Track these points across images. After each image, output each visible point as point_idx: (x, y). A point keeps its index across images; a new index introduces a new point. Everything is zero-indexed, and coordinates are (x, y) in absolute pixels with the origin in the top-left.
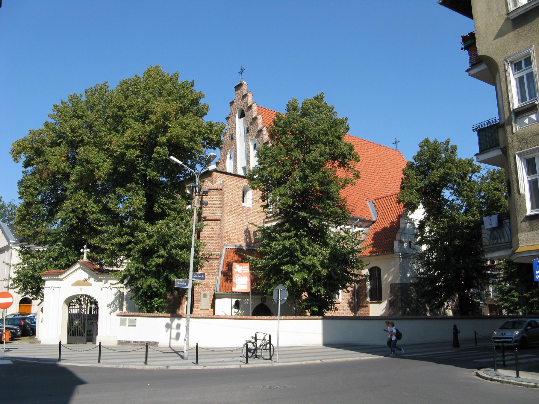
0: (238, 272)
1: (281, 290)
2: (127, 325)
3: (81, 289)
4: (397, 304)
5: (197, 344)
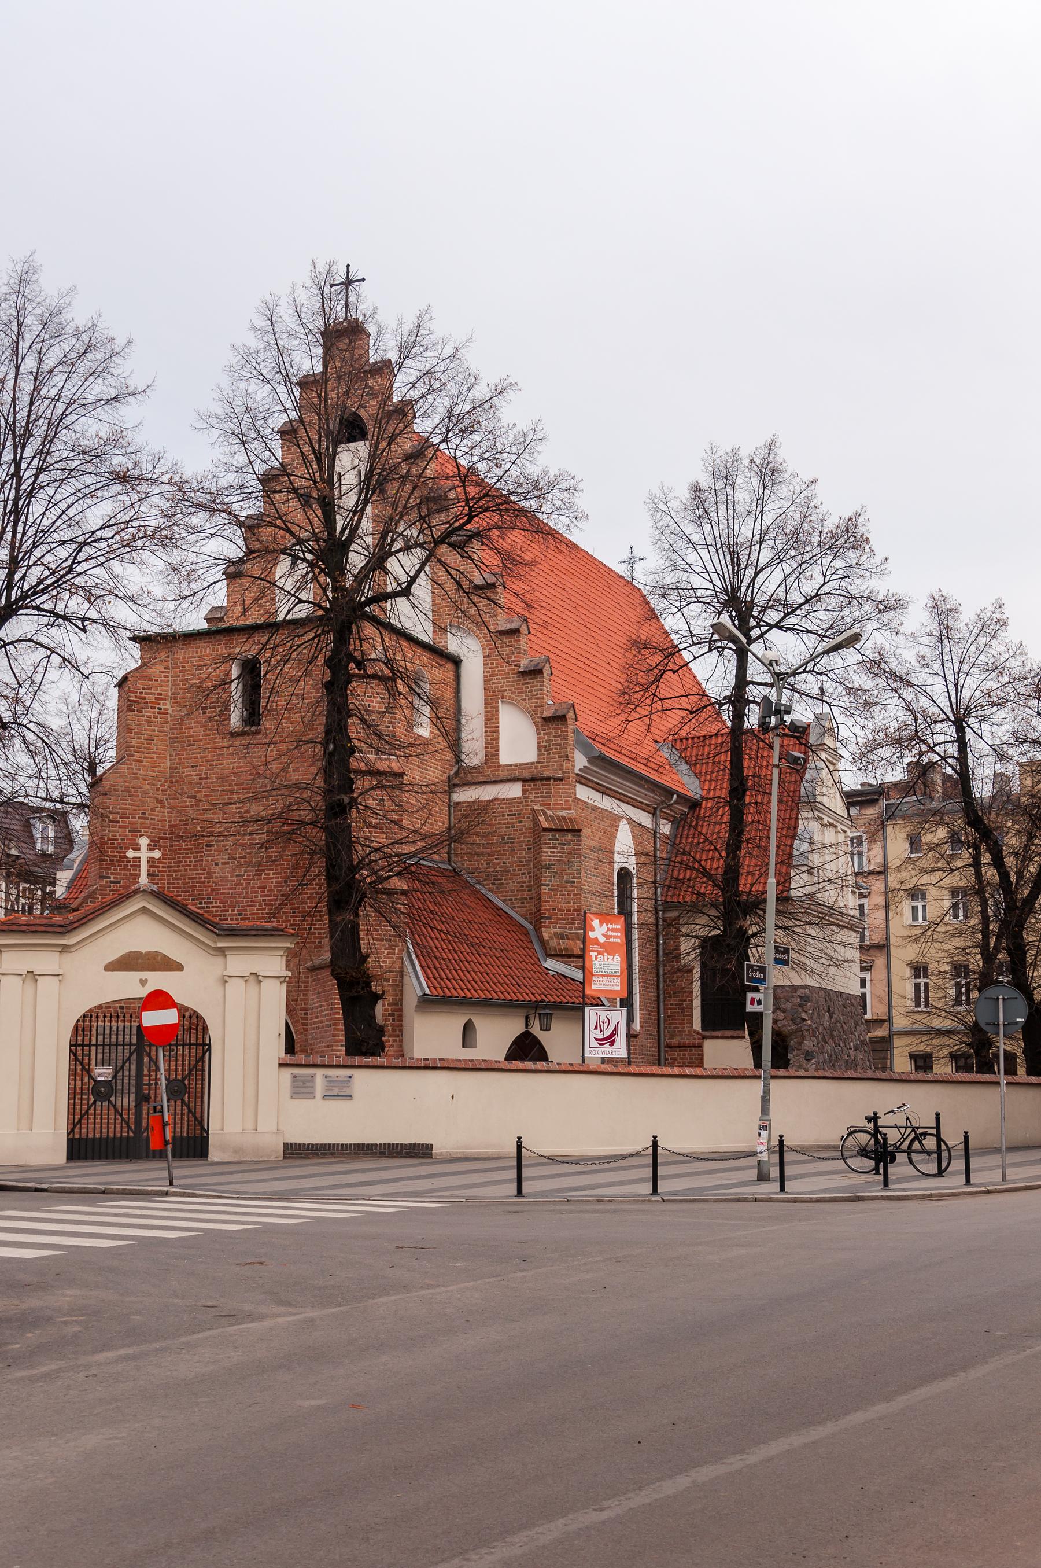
0: (596, 941)
1: (1004, 999)
4: (800, 1043)
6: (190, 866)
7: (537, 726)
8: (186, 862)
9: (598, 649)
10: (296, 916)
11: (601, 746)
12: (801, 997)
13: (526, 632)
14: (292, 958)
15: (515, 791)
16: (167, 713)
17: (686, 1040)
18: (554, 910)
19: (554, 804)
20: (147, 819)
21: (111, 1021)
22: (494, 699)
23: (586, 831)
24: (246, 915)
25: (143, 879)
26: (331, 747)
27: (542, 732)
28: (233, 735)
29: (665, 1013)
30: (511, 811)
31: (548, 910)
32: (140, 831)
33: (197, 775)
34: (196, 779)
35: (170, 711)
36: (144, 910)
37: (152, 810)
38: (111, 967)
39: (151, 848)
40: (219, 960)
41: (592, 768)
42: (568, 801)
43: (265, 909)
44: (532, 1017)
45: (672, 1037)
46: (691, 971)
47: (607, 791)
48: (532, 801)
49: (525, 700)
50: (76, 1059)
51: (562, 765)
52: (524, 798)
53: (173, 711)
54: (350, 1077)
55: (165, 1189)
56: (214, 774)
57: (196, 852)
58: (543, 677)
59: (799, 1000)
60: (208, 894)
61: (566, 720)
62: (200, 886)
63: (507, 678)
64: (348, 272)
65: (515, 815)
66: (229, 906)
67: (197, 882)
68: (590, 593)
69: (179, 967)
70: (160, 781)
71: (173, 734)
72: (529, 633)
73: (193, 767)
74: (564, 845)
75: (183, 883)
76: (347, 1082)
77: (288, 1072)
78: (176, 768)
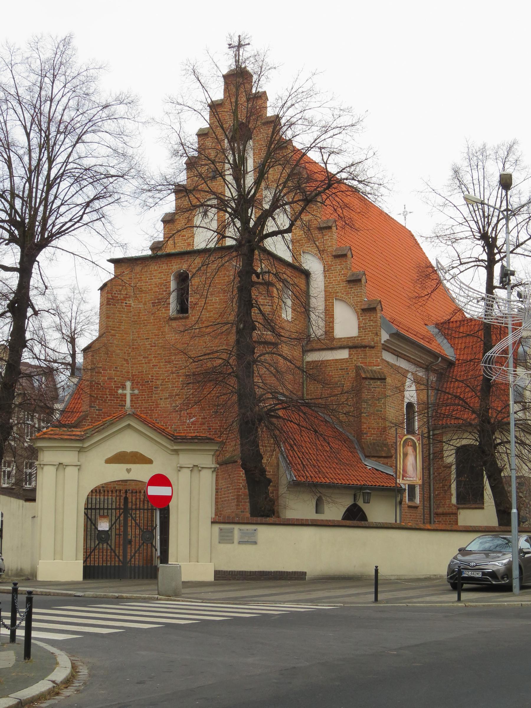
2: (236, 540)
3: (128, 471)
5: (377, 567)
6: (144, 400)
7: (358, 314)
8: (142, 398)
9: (389, 267)
10: (211, 432)
11: (397, 327)
13: (351, 256)
14: (217, 455)
15: (344, 354)
16: (131, 306)
17: (446, 510)
18: (369, 428)
19: (369, 363)
20: (118, 371)
21: (96, 495)
22: (331, 298)
23: (389, 380)
24: (179, 430)
25: (416, 409)
26: (242, 326)
27: (361, 318)
28: (171, 319)
29: (434, 493)
30: (342, 367)
31: (366, 429)
32: (114, 379)
33: (149, 344)
34: (149, 347)
35: (132, 305)
36: (129, 426)
37: (122, 366)
38: (109, 461)
39: (132, 389)
40: (174, 457)
41: (392, 340)
42: (377, 361)
43: (191, 427)
44: (358, 495)
45: (438, 507)
46: (450, 467)
47: (400, 355)
48: (355, 361)
49: (350, 298)
50: (88, 517)
51: (374, 339)
52: (350, 359)
53: (134, 305)
54: (255, 530)
55: (156, 596)
57: (149, 392)
58: (362, 284)
60: (156, 418)
61: (376, 310)
62: (151, 413)
63: (338, 285)
65: (344, 369)
66: (169, 425)
67: (149, 410)
68: (382, 233)
70: (126, 348)
71: (134, 318)
72: (352, 257)
73: (146, 339)
74: (375, 388)
75: (140, 411)
77: (216, 527)
78: (136, 340)
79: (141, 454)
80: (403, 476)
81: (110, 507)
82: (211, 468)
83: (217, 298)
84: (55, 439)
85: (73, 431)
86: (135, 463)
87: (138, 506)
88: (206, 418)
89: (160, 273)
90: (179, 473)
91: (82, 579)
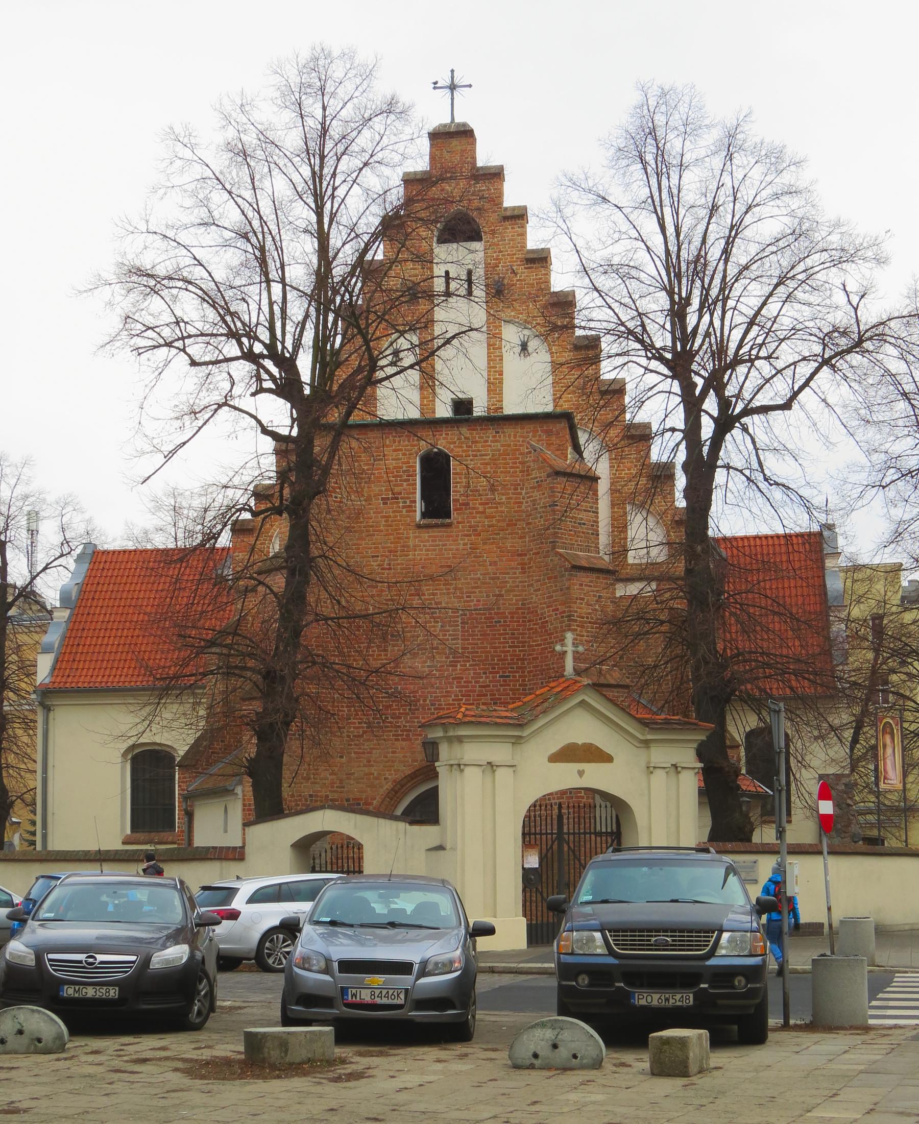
3: (581, 773)
12: (846, 785)
36: (583, 703)
38: (553, 758)
56: (398, 564)
59: (843, 787)
64: (452, 78)
69: (608, 759)
73: (373, 557)
76: (752, 867)
79: (597, 748)
80: (885, 778)
81: (533, 830)
82: (694, 768)
83: (504, 497)
84: (487, 724)
85: (495, 710)
86: (589, 761)
87: (538, 829)
88: (489, 686)
89: (394, 450)
90: (652, 776)
91: (525, 947)
